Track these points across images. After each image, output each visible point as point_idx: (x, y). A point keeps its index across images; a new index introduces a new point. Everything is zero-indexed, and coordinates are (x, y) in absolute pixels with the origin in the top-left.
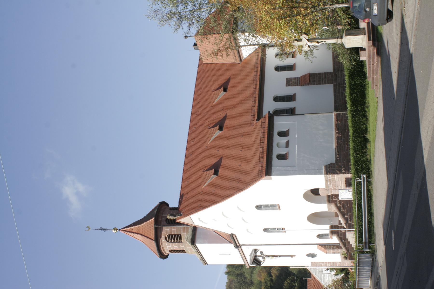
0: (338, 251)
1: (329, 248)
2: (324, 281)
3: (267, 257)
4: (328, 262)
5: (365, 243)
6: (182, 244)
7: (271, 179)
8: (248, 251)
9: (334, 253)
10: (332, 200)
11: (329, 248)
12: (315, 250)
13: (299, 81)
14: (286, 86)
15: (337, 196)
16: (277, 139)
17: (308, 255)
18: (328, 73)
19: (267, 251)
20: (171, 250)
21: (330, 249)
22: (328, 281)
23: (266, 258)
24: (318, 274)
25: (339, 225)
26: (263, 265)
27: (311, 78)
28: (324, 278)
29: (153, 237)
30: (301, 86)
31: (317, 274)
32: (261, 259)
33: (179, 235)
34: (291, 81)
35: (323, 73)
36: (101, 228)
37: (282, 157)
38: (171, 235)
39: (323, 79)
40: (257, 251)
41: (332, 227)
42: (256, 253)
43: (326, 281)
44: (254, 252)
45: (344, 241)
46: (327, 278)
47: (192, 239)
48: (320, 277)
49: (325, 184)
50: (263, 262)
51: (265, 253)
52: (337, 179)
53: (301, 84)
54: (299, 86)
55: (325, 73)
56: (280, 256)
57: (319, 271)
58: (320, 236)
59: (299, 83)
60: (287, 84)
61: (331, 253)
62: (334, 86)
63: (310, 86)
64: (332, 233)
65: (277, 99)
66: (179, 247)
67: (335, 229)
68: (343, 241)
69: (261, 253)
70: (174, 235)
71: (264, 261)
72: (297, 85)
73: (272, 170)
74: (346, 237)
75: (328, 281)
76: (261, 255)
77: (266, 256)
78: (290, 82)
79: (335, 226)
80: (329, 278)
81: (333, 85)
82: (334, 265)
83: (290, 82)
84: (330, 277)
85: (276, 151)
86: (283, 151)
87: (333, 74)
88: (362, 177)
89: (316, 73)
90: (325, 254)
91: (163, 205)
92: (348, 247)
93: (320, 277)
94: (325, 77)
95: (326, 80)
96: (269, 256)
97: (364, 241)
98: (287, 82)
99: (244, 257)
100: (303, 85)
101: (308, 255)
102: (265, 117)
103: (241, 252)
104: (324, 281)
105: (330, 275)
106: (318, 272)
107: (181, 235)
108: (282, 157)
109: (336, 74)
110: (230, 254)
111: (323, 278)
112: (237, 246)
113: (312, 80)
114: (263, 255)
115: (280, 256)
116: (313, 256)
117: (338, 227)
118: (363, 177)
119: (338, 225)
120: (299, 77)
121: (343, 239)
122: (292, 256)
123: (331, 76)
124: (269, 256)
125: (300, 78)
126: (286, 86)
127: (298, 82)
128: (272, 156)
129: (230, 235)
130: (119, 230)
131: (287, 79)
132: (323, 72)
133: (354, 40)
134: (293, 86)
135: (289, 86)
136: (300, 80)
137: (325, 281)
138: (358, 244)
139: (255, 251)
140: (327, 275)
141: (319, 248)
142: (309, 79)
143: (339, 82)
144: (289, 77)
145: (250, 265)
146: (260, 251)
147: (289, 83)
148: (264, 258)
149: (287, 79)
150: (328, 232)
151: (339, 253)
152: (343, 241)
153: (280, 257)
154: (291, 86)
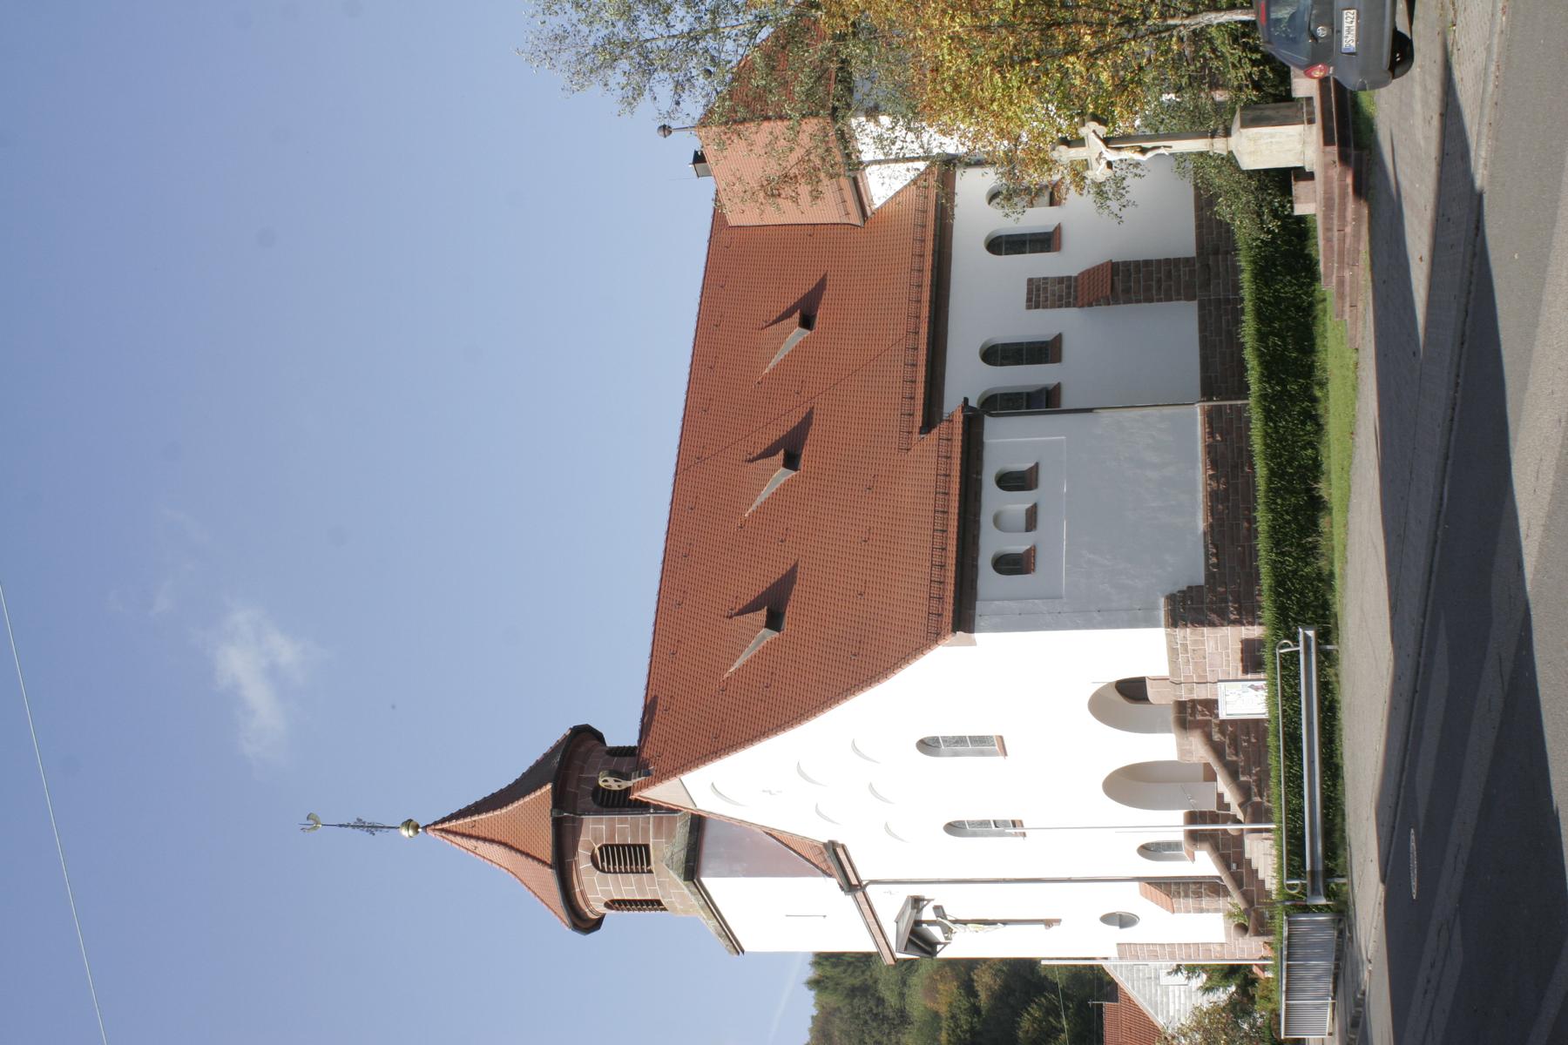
0: (1214, 906)
1: (1182, 894)
2: (1165, 1012)
3: (958, 926)
4: (1180, 944)
5: (1313, 873)
6: (653, 879)
7: (973, 643)
8: (890, 905)
9: (1201, 911)
10: (1192, 718)
11: (1182, 894)
12: (1130, 899)
13: (1075, 291)
14: (1029, 307)
15: (1211, 705)
16: (994, 500)
17: (1107, 919)
18: (1177, 261)
19: (957, 903)
20: (613, 901)
21: (1186, 896)
22: (1179, 1010)
23: (957, 928)
24: (1144, 985)
25: (1219, 809)
26: (944, 953)
27: (1115, 278)
28: (1165, 1000)
29: (547, 853)
30: (1082, 306)
31: (1139, 988)
32: (936, 932)
33: (640, 846)
34: (1046, 288)
35: (1159, 262)
36: (359, 820)
37: (1012, 564)
38: (612, 846)
39: (1159, 281)
40: (921, 904)
41: (1192, 818)
42: (919, 910)
43: (1171, 1014)
44: (913, 908)
45: (1238, 868)
46: (1177, 999)
47: (687, 861)
48: (1150, 998)
49: (1169, 660)
50: (945, 944)
51: (952, 912)
52: (1212, 643)
53: (1080, 299)
54: (1074, 306)
55: (1167, 261)
56: (1005, 922)
57: (1147, 976)
58: (1148, 850)
59: (1076, 298)
60: (1029, 300)
61: (1190, 912)
62: (1201, 307)
63: (1113, 308)
64: (1194, 837)
65: (994, 355)
66: (641, 889)
67: (1205, 823)
68: (1234, 866)
69: (938, 910)
70: (623, 846)
71: (947, 938)
72: (1068, 305)
73: (978, 611)
74: (1242, 853)
75: (1179, 1010)
76: (937, 917)
77: (956, 922)
78: (1040, 294)
79: (1206, 812)
80: (1182, 1002)
81: (1194, 305)
82: (1199, 955)
83: (1040, 294)
84: (1186, 997)
85: (992, 542)
86: (1017, 544)
87: (1197, 266)
88: (1301, 638)
89: (1135, 262)
90: (1168, 914)
91: (583, 738)
92: (1253, 891)
93: (1150, 998)
94: (1169, 275)
95: (1170, 286)
96: (965, 922)
97: (1308, 868)
98: (1030, 292)
99: (875, 927)
100: (1090, 305)
101: (1107, 919)
102: (951, 421)
103: (865, 907)
104: (1165, 1012)
105: (1185, 992)
106: (1144, 980)
107: (647, 847)
108: (1012, 564)
109: (1208, 265)
110: (825, 916)
111: (1162, 1003)
112: (852, 886)
113: (1120, 287)
114: (944, 917)
115: (1005, 922)
116: (1123, 921)
117: (1214, 818)
118: (1307, 638)
119: (1214, 808)
120: (1074, 274)
121: (1234, 862)
122: (1048, 923)
123: (1190, 271)
124: (965, 922)
125: (1076, 278)
126: (1029, 307)
127: (1069, 294)
128: (975, 559)
129: (824, 844)
130: (425, 828)
131: (1030, 281)
132: (1162, 256)
133: (1273, 140)
134: (1053, 306)
135: (1037, 307)
136: (1076, 287)
137: (1168, 1012)
138: (1288, 879)
139: (917, 902)
140: (1174, 991)
141: (1144, 894)
142: (1109, 282)
143: (1219, 295)
144: (1039, 274)
145: (899, 956)
146: (932, 904)
147: (1038, 296)
148: (947, 931)
149: (1030, 281)
150: (1178, 835)
151: (1217, 910)
152: (1234, 866)
153: (1007, 926)
154: (1043, 308)
